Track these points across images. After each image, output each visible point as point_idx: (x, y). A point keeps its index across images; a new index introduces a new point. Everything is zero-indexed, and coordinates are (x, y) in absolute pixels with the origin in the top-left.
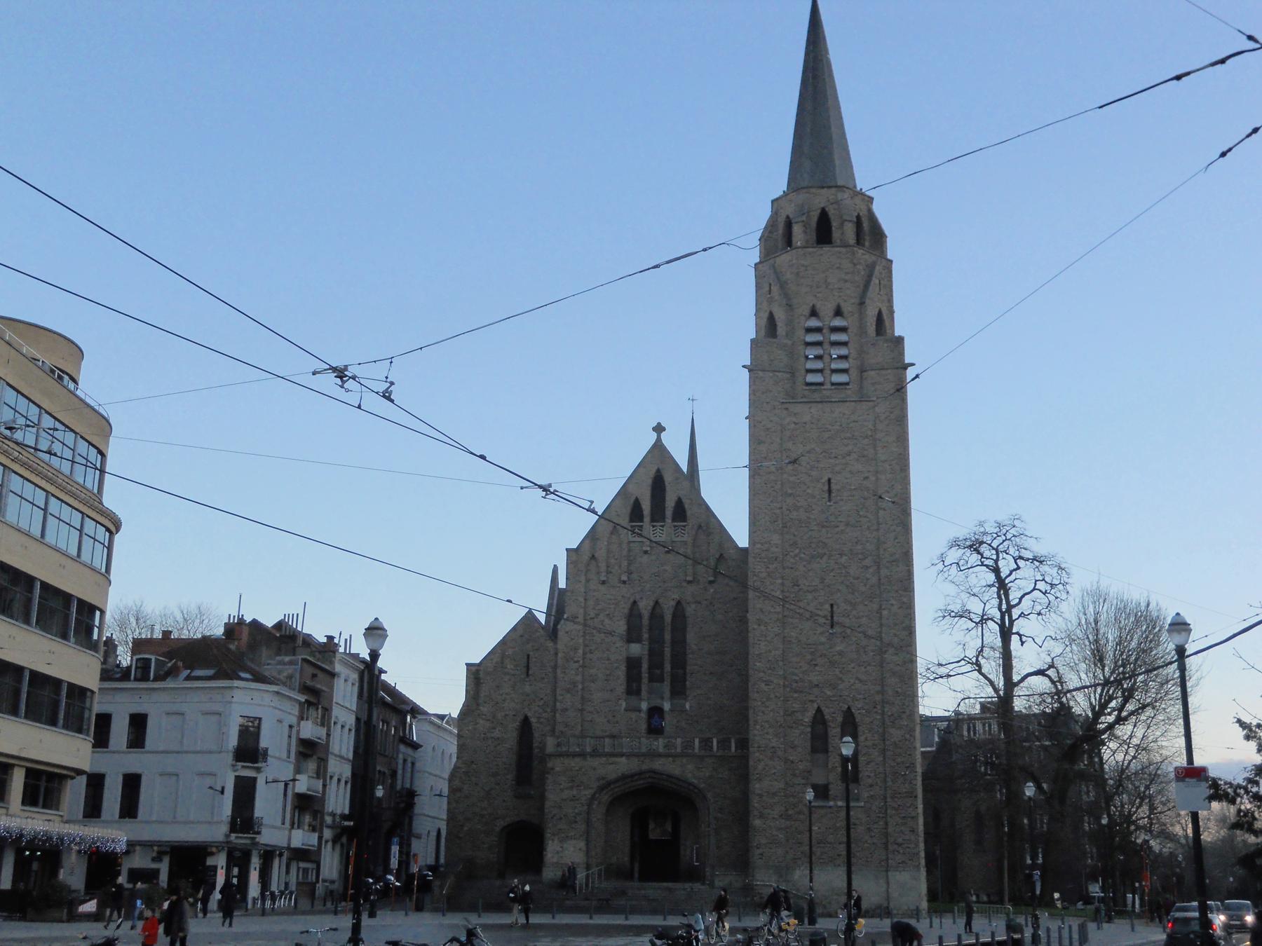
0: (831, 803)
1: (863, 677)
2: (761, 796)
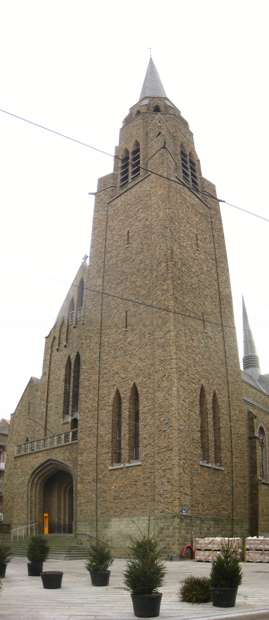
0: (210, 465)
1: (143, 356)
2: (82, 466)
